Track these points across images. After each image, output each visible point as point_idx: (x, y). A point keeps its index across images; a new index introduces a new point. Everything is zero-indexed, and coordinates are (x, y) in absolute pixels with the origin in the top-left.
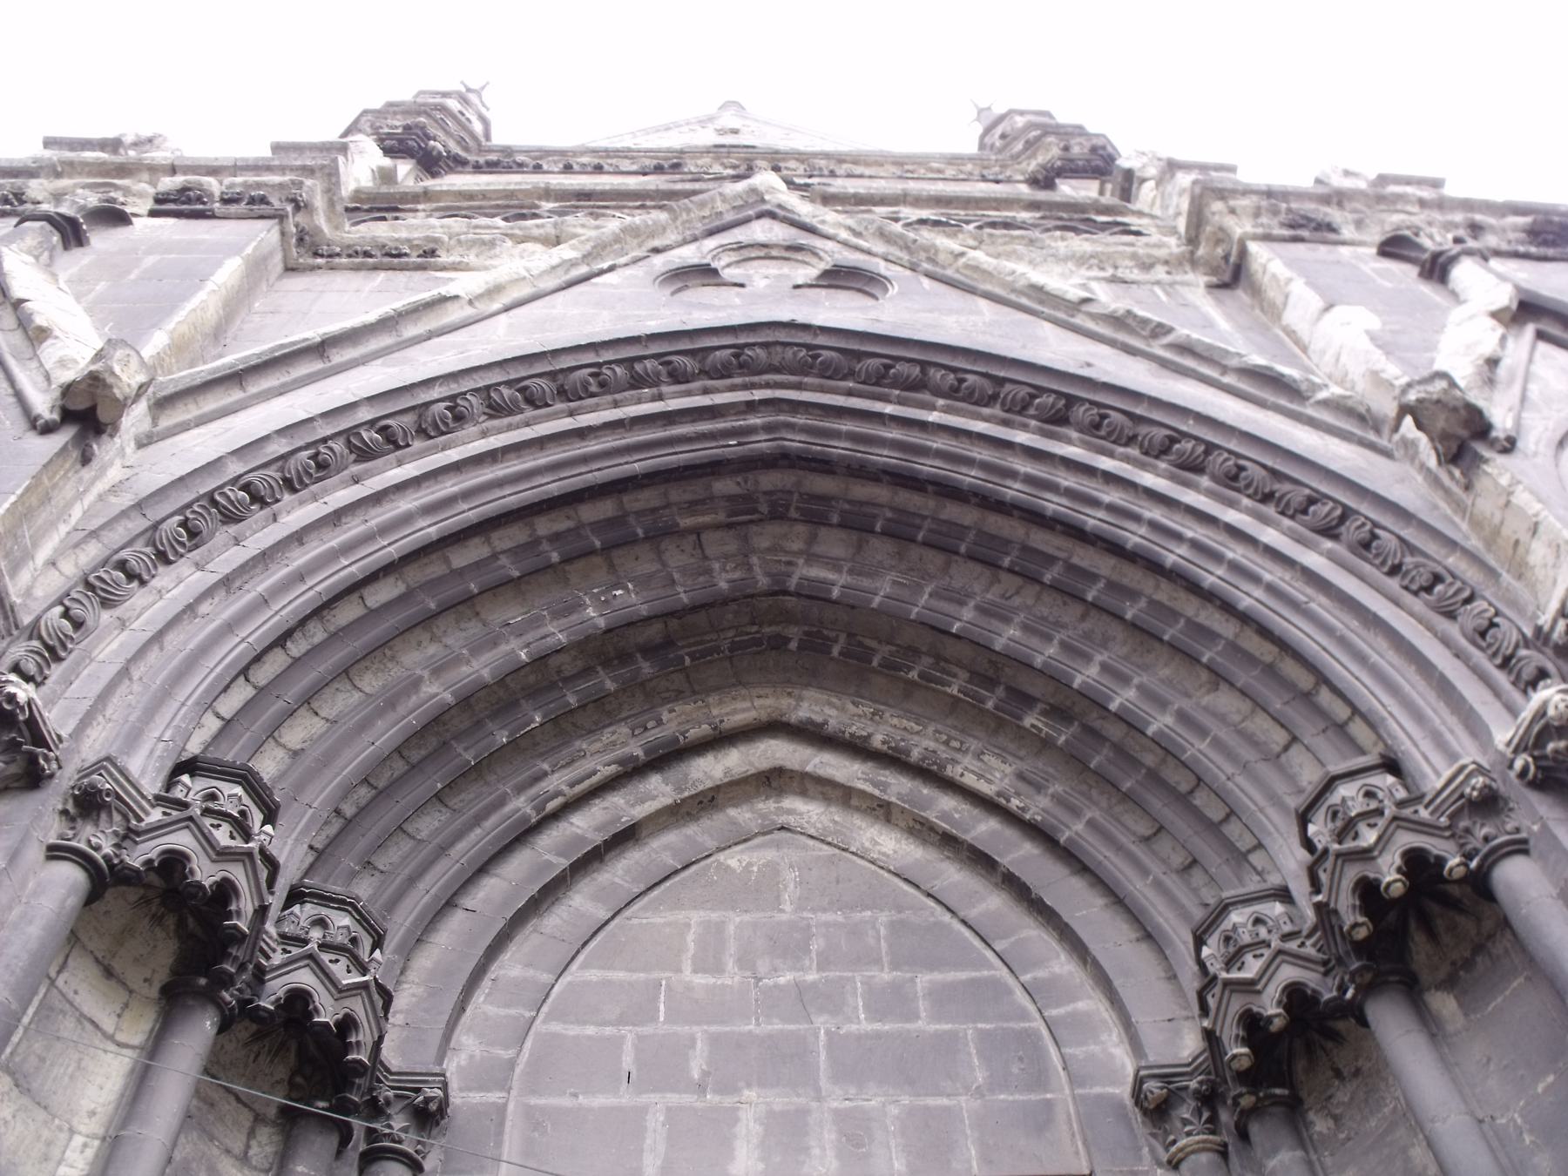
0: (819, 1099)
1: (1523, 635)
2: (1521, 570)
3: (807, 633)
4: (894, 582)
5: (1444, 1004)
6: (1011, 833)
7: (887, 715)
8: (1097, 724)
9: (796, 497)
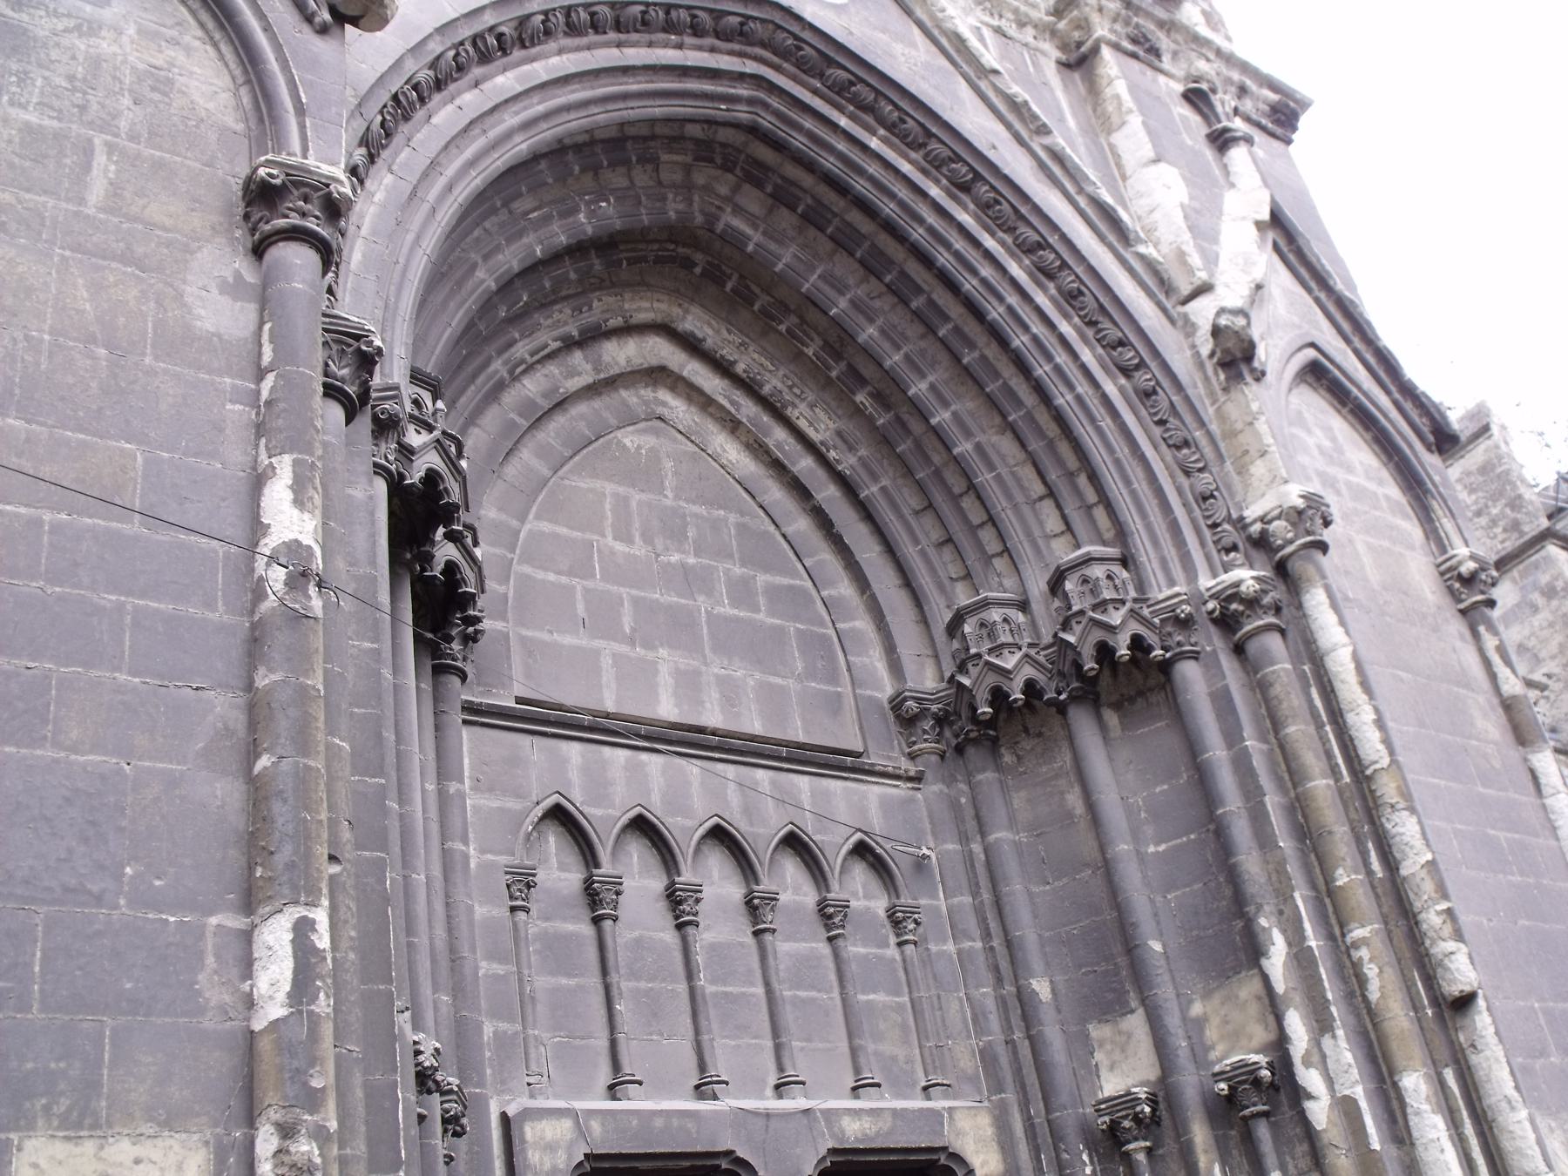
0: (706, 664)
1: (1230, 514)
2: (1242, 471)
3: (708, 263)
4: (795, 256)
5: (1111, 717)
6: (821, 473)
7: (751, 349)
8: (906, 417)
9: (743, 157)
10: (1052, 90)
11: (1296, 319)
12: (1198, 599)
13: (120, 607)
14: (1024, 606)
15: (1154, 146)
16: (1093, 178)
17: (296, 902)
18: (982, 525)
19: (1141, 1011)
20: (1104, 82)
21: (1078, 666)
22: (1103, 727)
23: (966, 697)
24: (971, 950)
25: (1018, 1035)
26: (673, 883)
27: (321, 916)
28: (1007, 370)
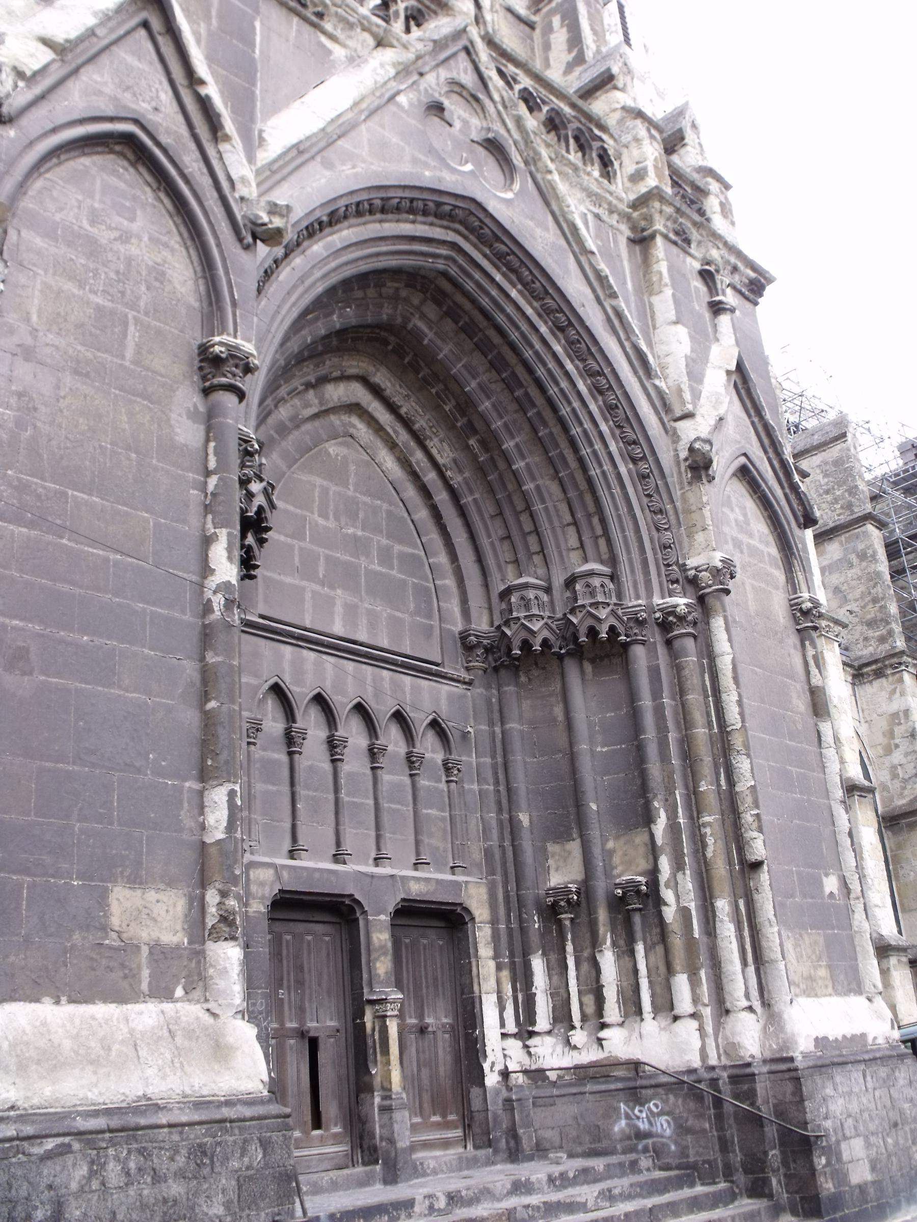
5: (588, 667)
6: (439, 483)
8: (496, 457)
10: (621, 261)
11: (738, 437)
12: (651, 609)
13: (144, 610)
14: (548, 590)
15: (677, 312)
16: (637, 332)
17: (229, 781)
18: (531, 532)
19: (578, 840)
20: (654, 260)
21: (575, 638)
22: (583, 672)
23: (506, 641)
24: (487, 790)
25: (507, 843)
26: (333, 735)
27: (237, 788)
28: (564, 444)
